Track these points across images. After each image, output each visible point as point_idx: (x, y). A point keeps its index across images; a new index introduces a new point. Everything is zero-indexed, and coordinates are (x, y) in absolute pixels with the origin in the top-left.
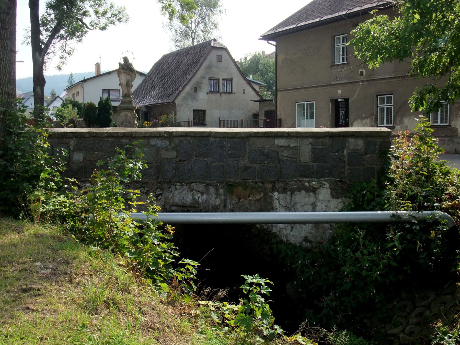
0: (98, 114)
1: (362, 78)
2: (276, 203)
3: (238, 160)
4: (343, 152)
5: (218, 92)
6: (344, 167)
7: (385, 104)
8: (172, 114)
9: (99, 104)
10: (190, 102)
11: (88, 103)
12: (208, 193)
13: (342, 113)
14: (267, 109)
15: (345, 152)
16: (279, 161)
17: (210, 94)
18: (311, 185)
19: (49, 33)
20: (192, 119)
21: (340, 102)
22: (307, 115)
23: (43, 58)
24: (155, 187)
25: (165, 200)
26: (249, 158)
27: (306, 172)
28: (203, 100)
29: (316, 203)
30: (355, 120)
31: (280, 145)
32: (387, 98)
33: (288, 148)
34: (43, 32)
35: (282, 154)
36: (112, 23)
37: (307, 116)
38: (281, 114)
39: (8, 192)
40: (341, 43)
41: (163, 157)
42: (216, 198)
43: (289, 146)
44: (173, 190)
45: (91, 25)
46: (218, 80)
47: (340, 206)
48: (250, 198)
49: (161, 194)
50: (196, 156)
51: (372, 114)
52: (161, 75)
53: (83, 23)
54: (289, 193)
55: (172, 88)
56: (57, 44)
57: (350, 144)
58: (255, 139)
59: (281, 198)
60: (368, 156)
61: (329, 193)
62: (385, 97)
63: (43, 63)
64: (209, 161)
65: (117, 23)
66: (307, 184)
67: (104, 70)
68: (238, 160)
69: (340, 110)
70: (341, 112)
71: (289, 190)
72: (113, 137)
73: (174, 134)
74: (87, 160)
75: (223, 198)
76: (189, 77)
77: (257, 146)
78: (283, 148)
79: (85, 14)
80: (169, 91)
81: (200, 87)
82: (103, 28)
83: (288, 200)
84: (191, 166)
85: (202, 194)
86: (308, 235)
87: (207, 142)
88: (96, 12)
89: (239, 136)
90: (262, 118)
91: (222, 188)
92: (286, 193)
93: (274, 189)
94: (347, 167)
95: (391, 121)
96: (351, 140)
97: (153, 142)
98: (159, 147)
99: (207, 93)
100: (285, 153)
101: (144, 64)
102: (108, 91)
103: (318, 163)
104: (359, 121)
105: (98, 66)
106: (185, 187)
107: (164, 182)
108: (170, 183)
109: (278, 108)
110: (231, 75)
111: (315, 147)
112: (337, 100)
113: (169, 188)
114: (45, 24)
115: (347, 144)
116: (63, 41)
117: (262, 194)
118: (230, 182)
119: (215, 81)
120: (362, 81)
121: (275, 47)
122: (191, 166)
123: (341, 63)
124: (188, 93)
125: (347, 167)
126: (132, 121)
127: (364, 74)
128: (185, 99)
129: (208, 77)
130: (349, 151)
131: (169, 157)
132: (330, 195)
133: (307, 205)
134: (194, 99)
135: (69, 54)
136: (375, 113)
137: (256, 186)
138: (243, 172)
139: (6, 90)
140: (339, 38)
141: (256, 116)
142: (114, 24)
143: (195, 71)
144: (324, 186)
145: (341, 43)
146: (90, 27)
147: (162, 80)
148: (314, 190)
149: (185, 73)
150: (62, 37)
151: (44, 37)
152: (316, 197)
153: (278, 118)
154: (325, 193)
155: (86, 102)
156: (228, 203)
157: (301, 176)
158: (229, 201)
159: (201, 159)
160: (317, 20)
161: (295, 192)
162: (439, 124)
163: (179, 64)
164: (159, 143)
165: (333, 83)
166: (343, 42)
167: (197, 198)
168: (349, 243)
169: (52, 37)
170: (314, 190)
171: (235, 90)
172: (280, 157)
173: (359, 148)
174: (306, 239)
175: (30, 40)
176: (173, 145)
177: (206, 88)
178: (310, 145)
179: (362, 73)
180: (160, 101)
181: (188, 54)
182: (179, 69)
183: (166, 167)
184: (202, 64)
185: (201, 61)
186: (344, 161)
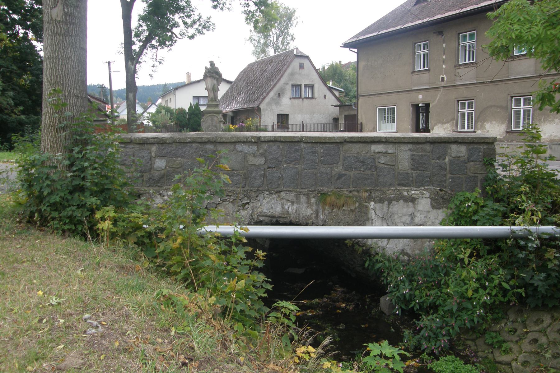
0: (190, 119)
1: (443, 84)
2: (372, 214)
3: (331, 168)
4: (445, 159)
5: (301, 97)
6: (445, 176)
7: (466, 109)
8: (257, 117)
9: (189, 110)
10: (274, 107)
11: (179, 109)
12: (298, 202)
13: (423, 117)
14: (347, 113)
15: (447, 160)
16: (376, 168)
17: (293, 100)
18: (410, 194)
19: (141, 44)
20: (275, 123)
21: (421, 106)
22: (388, 119)
23: (135, 67)
24: (242, 196)
25: (253, 210)
26: (343, 165)
27: (406, 181)
28: (286, 105)
29: (415, 214)
30: (436, 124)
31: (377, 151)
32: (469, 103)
33: (386, 155)
34: (137, 42)
35: (379, 161)
36: (200, 32)
37: (388, 120)
38: (362, 118)
39: (74, 208)
40: (422, 50)
41: (250, 163)
42: (308, 207)
43: (386, 153)
44: (261, 200)
45: (181, 35)
46: (300, 86)
47: (441, 218)
48: (344, 208)
49: (248, 203)
50: (286, 162)
51: (453, 119)
52: (246, 82)
53: (173, 33)
54: (386, 202)
55: (257, 93)
56: (148, 53)
57: (453, 150)
58: (350, 145)
59: (378, 208)
60: (472, 163)
61: (429, 203)
62: (466, 102)
63: (135, 72)
64: (300, 169)
65: (205, 31)
66: (405, 193)
67: (193, 79)
68: (331, 168)
69: (421, 114)
70: (421, 117)
71: (386, 200)
72: (197, 142)
73: (262, 139)
74: (169, 167)
75: (314, 207)
76: (273, 83)
77: (352, 152)
78: (380, 154)
79: (175, 25)
80: (255, 97)
81: (283, 93)
82: (192, 37)
83: (385, 210)
84: (281, 174)
85: (293, 203)
86: (406, 247)
87: (297, 147)
88: (185, 23)
89: (333, 141)
90: (342, 122)
91: (314, 197)
92: (383, 203)
93: (370, 199)
94: (449, 176)
95: (472, 126)
96: (454, 147)
97: (239, 147)
98: (246, 153)
99: (290, 99)
100: (383, 160)
101: (231, 72)
102: (198, 98)
103: (418, 171)
104: (440, 125)
105: (189, 74)
106: (274, 196)
107: (252, 190)
108: (259, 191)
109: (359, 112)
110: (313, 81)
111: (414, 153)
112: (418, 105)
113: (257, 196)
114: (137, 35)
115: (449, 151)
116: (154, 51)
117: (357, 205)
118: (323, 190)
119: (297, 87)
120: (444, 87)
121: (356, 54)
122: (281, 174)
123: (422, 69)
124: (272, 99)
125: (449, 176)
126: (218, 125)
127: (445, 79)
128: (269, 104)
129: (291, 83)
130: (451, 158)
131: (257, 164)
132: (429, 205)
133: (405, 215)
134: (278, 104)
135: (160, 63)
136: (456, 118)
137: (351, 195)
138: (337, 180)
139: (75, 91)
140: (420, 45)
141: (336, 120)
142: (202, 34)
143: (278, 78)
144: (423, 196)
145: (422, 50)
146: (179, 36)
147: (247, 87)
148: (413, 200)
149: (269, 79)
150: (153, 47)
151: (136, 47)
152: (415, 208)
153: (360, 122)
154: (424, 203)
155: (177, 108)
156: (320, 213)
157: (399, 185)
158: (321, 211)
159: (291, 166)
160: (399, 27)
161: (393, 202)
162: (466, 129)
163: (263, 72)
164: (246, 148)
165: (413, 89)
166: (424, 49)
167: (286, 207)
168: (453, 259)
169: (143, 48)
170: (413, 200)
171: (316, 95)
172: (377, 164)
173: (462, 155)
174: (403, 252)
175: (123, 50)
176: (261, 151)
177: (289, 93)
178: (409, 152)
179: (443, 79)
180: (246, 106)
181: (272, 62)
182: (261, 78)
183: (254, 174)
184: (285, 71)
185: (284, 69)
186: (446, 170)
